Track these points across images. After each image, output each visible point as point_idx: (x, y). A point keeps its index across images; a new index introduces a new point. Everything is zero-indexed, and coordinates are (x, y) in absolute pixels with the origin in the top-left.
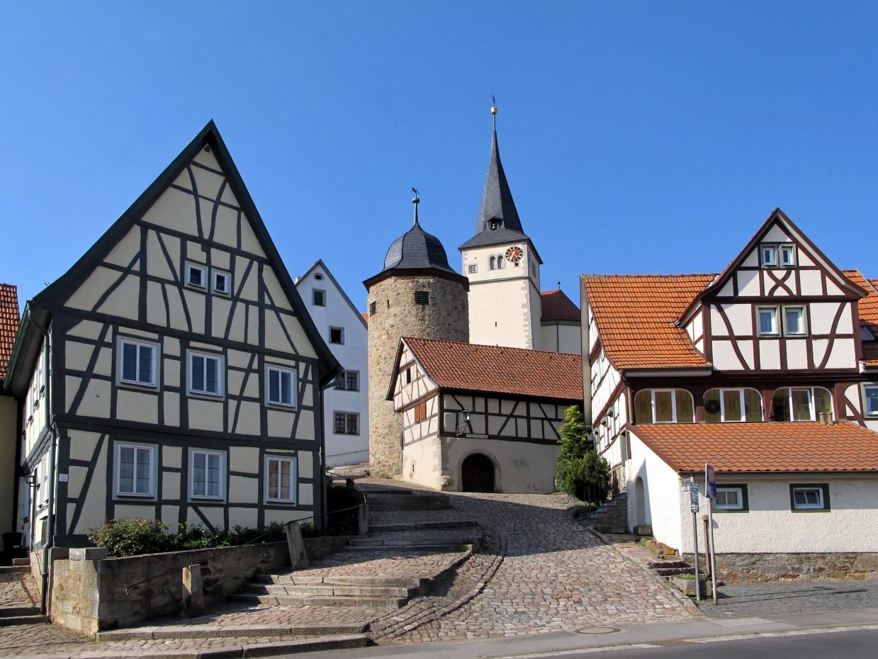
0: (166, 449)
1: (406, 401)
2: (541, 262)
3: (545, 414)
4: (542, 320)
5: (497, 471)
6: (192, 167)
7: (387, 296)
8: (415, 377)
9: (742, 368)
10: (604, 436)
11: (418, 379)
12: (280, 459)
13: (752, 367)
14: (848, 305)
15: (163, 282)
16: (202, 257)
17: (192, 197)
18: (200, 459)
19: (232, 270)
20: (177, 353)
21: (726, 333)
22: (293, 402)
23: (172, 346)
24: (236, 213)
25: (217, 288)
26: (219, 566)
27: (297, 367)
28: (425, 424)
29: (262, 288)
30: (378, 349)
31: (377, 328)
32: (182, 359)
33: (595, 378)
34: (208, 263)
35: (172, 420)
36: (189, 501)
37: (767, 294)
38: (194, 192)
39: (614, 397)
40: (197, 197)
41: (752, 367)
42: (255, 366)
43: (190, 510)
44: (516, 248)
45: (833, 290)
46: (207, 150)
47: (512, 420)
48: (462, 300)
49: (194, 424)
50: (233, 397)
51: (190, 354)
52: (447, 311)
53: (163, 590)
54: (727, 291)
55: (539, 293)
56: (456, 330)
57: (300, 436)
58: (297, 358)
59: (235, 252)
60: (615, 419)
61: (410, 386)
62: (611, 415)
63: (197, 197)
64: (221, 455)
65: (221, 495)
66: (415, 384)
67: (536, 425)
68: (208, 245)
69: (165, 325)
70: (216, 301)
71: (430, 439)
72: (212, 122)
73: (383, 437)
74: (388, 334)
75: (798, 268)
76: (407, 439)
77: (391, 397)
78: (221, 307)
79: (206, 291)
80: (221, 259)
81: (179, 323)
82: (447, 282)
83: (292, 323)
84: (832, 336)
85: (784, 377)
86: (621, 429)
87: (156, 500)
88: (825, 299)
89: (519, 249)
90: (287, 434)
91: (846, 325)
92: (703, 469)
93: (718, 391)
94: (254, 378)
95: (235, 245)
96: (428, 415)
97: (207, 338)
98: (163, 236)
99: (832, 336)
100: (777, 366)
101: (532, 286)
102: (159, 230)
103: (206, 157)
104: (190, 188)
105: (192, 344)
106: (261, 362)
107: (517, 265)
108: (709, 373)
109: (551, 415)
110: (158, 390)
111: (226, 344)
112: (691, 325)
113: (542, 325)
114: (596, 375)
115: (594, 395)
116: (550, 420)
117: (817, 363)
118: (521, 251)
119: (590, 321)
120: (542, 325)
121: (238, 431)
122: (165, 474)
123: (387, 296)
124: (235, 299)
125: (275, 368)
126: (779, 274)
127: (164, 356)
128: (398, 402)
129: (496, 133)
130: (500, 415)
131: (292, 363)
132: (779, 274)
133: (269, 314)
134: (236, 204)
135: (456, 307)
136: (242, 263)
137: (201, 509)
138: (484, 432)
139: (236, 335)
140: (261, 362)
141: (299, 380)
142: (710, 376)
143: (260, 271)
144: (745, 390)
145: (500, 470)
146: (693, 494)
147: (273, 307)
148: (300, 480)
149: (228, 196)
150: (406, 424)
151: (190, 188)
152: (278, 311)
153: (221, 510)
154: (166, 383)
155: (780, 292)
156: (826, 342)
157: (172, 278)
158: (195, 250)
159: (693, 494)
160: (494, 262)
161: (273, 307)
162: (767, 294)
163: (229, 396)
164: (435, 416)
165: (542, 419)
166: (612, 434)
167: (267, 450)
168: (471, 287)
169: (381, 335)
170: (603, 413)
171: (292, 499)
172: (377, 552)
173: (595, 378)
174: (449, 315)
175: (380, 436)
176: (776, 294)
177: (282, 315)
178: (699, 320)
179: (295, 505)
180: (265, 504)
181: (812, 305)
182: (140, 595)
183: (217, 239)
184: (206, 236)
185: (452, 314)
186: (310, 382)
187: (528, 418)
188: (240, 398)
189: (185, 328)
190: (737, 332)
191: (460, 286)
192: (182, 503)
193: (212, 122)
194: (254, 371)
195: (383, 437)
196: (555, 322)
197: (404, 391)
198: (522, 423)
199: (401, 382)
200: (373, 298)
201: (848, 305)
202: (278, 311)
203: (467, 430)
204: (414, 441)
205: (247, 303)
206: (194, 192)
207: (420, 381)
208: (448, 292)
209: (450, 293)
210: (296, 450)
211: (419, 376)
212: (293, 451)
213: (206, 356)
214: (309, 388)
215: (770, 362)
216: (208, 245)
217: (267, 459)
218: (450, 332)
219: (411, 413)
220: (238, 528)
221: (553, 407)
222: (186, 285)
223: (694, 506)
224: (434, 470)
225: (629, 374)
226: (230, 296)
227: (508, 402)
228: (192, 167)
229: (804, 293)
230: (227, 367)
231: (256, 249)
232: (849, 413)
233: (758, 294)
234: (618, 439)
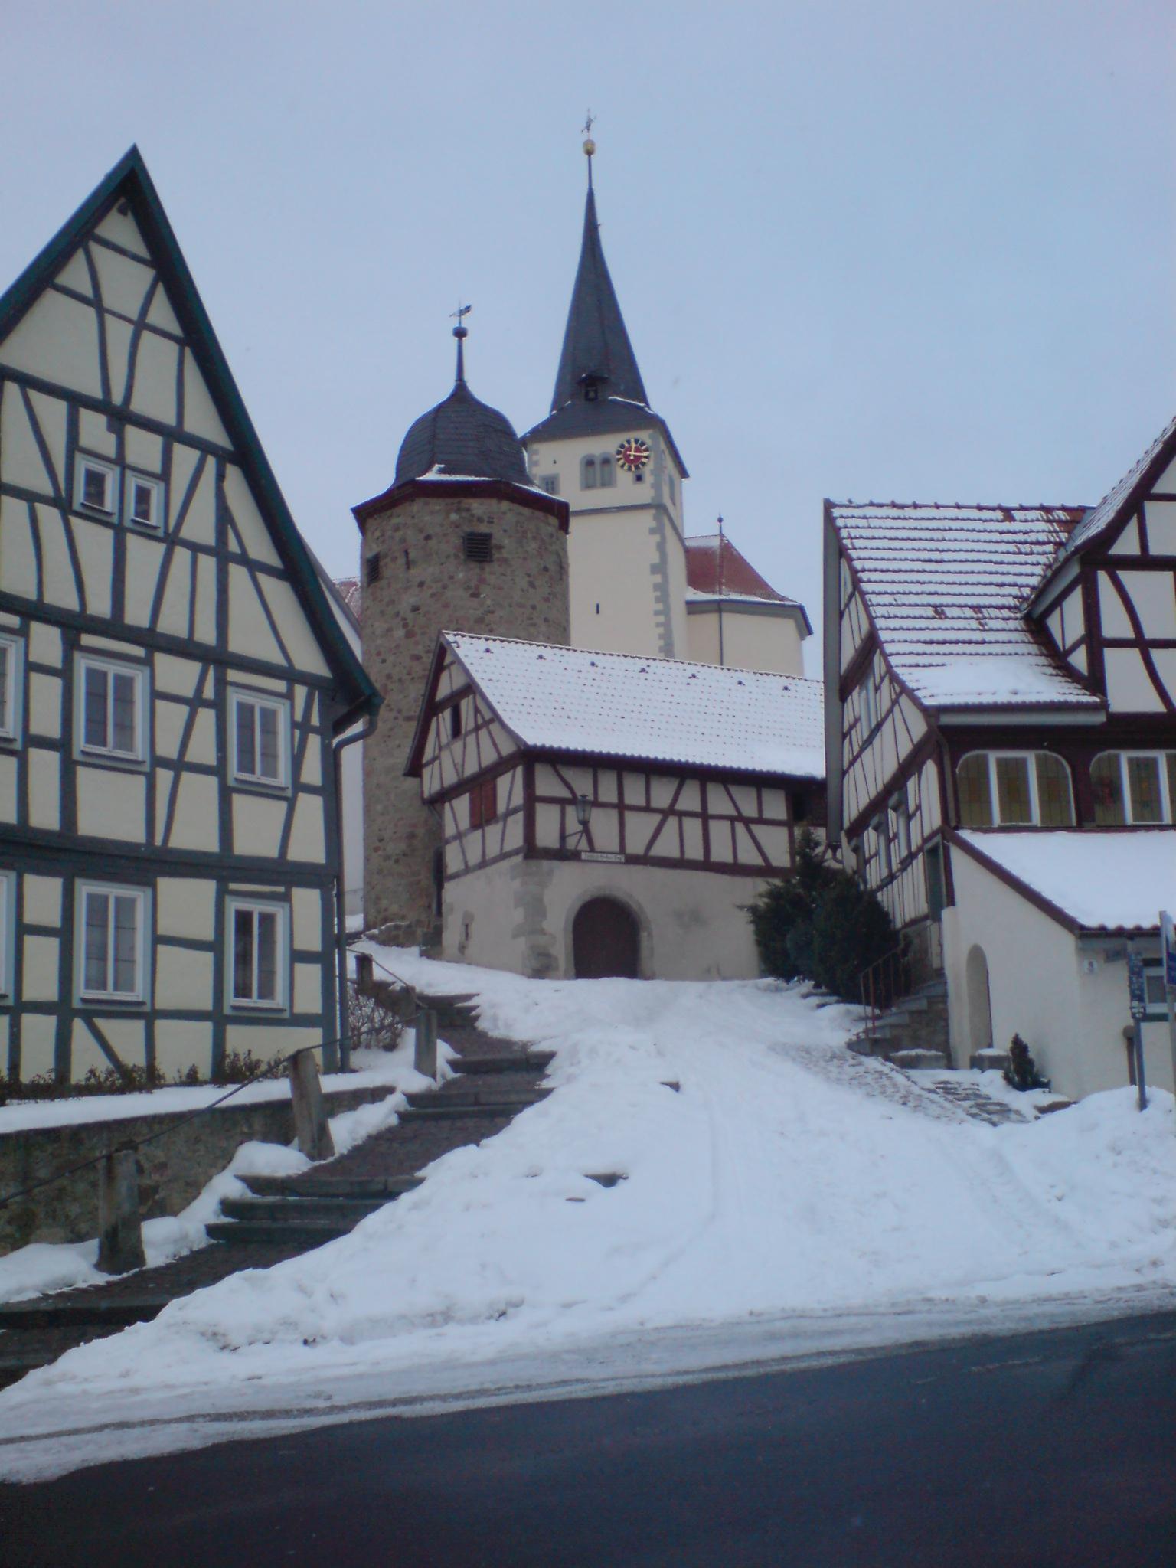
0: (31, 881)
1: (450, 778)
2: (684, 473)
3: (737, 809)
5: (644, 935)
6: (96, 249)
7: (403, 540)
8: (471, 725)
10: (877, 854)
11: (477, 728)
12: (256, 908)
15: (30, 497)
16: (107, 444)
17: (91, 313)
18: (97, 905)
19: (165, 476)
20: (55, 659)
21: (1130, 634)
22: (283, 778)
23: (46, 642)
24: (173, 348)
25: (137, 514)
26: (160, 1155)
27: (289, 696)
28: (493, 831)
29: (224, 518)
30: (384, 661)
31: (382, 613)
32: (65, 673)
33: (851, 727)
34: (120, 461)
35: (45, 816)
36: (76, 1004)
38: (95, 302)
39: (909, 768)
40: (101, 311)
42: (209, 692)
43: (79, 1026)
46: (123, 211)
47: (672, 822)
48: (558, 554)
49: (91, 824)
50: (165, 763)
51: (82, 664)
52: (529, 575)
53: (54, 1211)
54: (1127, 545)
55: (681, 540)
56: (546, 620)
57: (295, 854)
58: (290, 675)
59: (172, 435)
60: (909, 818)
61: (458, 746)
62: (901, 806)
63: (101, 311)
64: (140, 897)
65: (139, 992)
66: (471, 740)
67: (720, 831)
68: (120, 417)
69: (32, 596)
70: (132, 541)
71: (505, 864)
72: (134, 155)
73: (397, 861)
74: (405, 625)
76: (453, 861)
77: (415, 768)
78: (143, 555)
79: (115, 520)
80: (143, 448)
81: (61, 595)
82: (526, 511)
83: (279, 593)
86: (925, 840)
87: (10, 1002)
90: (269, 849)
92: (85, 991)
93: (1117, 759)
94: (206, 718)
95: (169, 419)
96: (501, 808)
97: (115, 627)
98: (33, 394)
101: (680, 530)
102: (28, 382)
103: (120, 228)
104: (87, 291)
105: (87, 640)
106: (221, 684)
107: (639, 478)
108: (1100, 718)
109: (749, 810)
110: (18, 746)
111: (153, 641)
112: (1057, 613)
114: (857, 720)
115: (852, 763)
116: (747, 822)
119: (844, 600)
121: (175, 842)
122: (29, 941)
123: (403, 540)
124: (172, 540)
125: (248, 698)
127: (31, 667)
128: (431, 782)
130: (647, 809)
131: (280, 686)
133: (238, 574)
134: (175, 328)
135: (546, 569)
136: (185, 458)
137: (100, 1022)
138: (616, 847)
139: (173, 623)
140: (221, 684)
141: (294, 725)
142: (1103, 725)
143: (221, 477)
144: (1038, 759)
145: (650, 935)
146: (1134, 979)
147: (244, 559)
148: (298, 956)
149: (162, 314)
150: (450, 830)
151: (87, 291)
152: (254, 567)
153: (139, 1025)
154: (35, 729)
157: (47, 489)
158: (94, 429)
159: (1134, 979)
160: (596, 471)
161: (244, 559)
163: (159, 762)
164: (515, 811)
165: (732, 819)
166: (899, 851)
167: (233, 886)
168: (574, 524)
169: (389, 630)
170: (878, 805)
171: (279, 1000)
172: (470, 1123)
173: (851, 727)
174: (532, 585)
175: (387, 858)
177: (262, 578)
178: (1074, 604)
179: (286, 1015)
180: (227, 1011)
182: (9, 1222)
183: (137, 406)
184: (117, 398)
185: (537, 583)
186: (315, 730)
187: (705, 816)
188: (179, 766)
189: (71, 603)
190: (1134, 654)
191: (554, 521)
192: (62, 1009)
193: (134, 155)
194: (207, 704)
195: (397, 861)
197: (445, 756)
198: (693, 827)
199: (438, 734)
200: (374, 546)
202: (254, 567)
203: (584, 845)
204: (467, 870)
205: (195, 548)
206: (95, 302)
207: (483, 733)
208: (529, 535)
209: (534, 538)
210: (290, 884)
211: (480, 721)
212: (281, 889)
213: (112, 669)
214: (314, 742)
216: (120, 417)
217: (233, 906)
218: (534, 625)
219: (462, 805)
220: (50, 1071)
221: (752, 793)
222: (76, 507)
223: (1136, 1003)
224: (515, 936)
225: (946, 720)
226: (160, 533)
227: (664, 780)
228: (96, 249)
230: (156, 695)
231: (210, 428)
234: (919, 863)
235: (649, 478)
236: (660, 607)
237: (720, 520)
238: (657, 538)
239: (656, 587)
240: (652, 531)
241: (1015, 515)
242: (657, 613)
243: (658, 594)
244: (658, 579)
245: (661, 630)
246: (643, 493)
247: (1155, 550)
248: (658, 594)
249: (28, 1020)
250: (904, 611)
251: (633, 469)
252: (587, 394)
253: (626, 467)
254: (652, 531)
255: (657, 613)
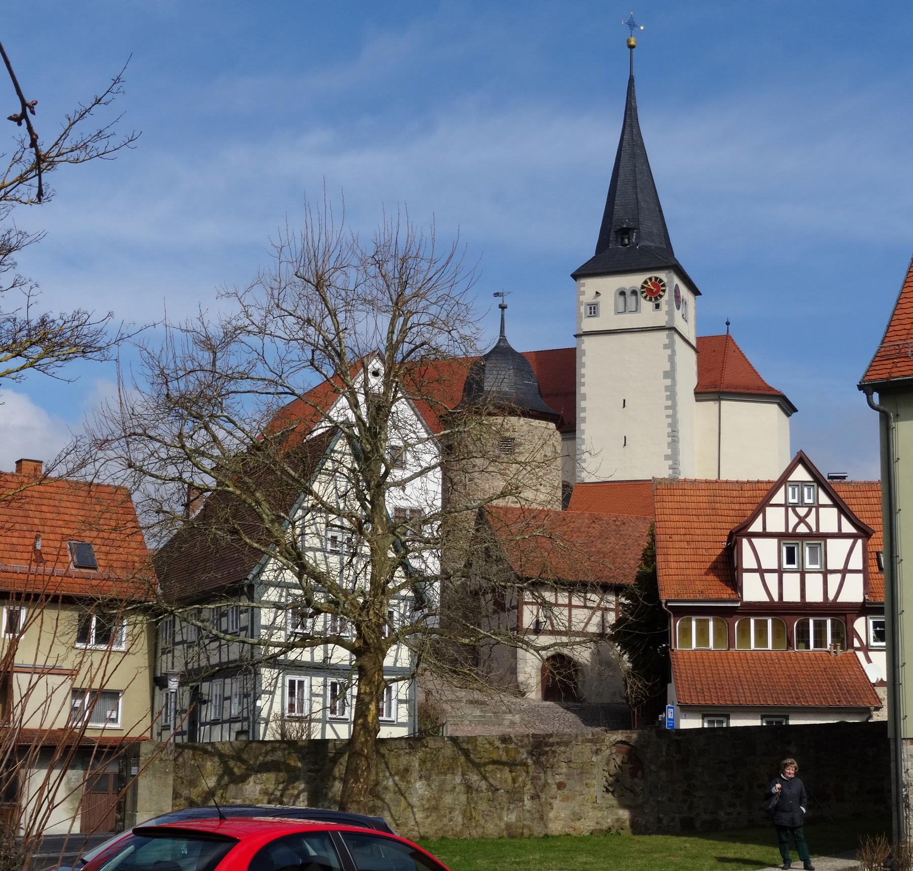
4: (696, 393)
9: (767, 599)
12: (297, 678)
13: (776, 599)
14: (860, 542)
37: (790, 530)
41: (776, 599)
44: (656, 278)
45: (848, 528)
75: (819, 506)
84: (845, 571)
85: (803, 609)
88: (840, 535)
89: (661, 281)
91: (857, 562)
99: (845, 571)
100: (797, 599)
107: (657, 306)
113: (697, 401)
117: (831, 596)
118: (664, 285)
120: (697, 401)
126: (802, 511)
129: (631, 80)
132: (802, 511)
148: (400, 701)
155: (802, 529)
156: (839, 576)
162: (790, 530)
171: (393, 718)
176: (829, 502)
181: (829, 541)
190: (757, 575)
196: (716, 397)
201: (860, 542)
215: (792, 595)
229: (822, 530)
232: (856, 644)
233: (783, 530)
235: (664, 307)
236: (669, 403)
237: (728, 324)
238: (669, 352)
239: (667, 388)
240: (666, 347)
241: (382, 737)
242: (667, 408)
243: (668, 393)
244: (668, 382)
245: (670, 420)
246: (661, 318)
247: (768, 530)
248: (668, 393)
249: (830, 577)
250: (719, 519)
251: (653, 299)
252: (623, 239)
253: (648, 298)
254: (666, 347)
255: (667, 408)
